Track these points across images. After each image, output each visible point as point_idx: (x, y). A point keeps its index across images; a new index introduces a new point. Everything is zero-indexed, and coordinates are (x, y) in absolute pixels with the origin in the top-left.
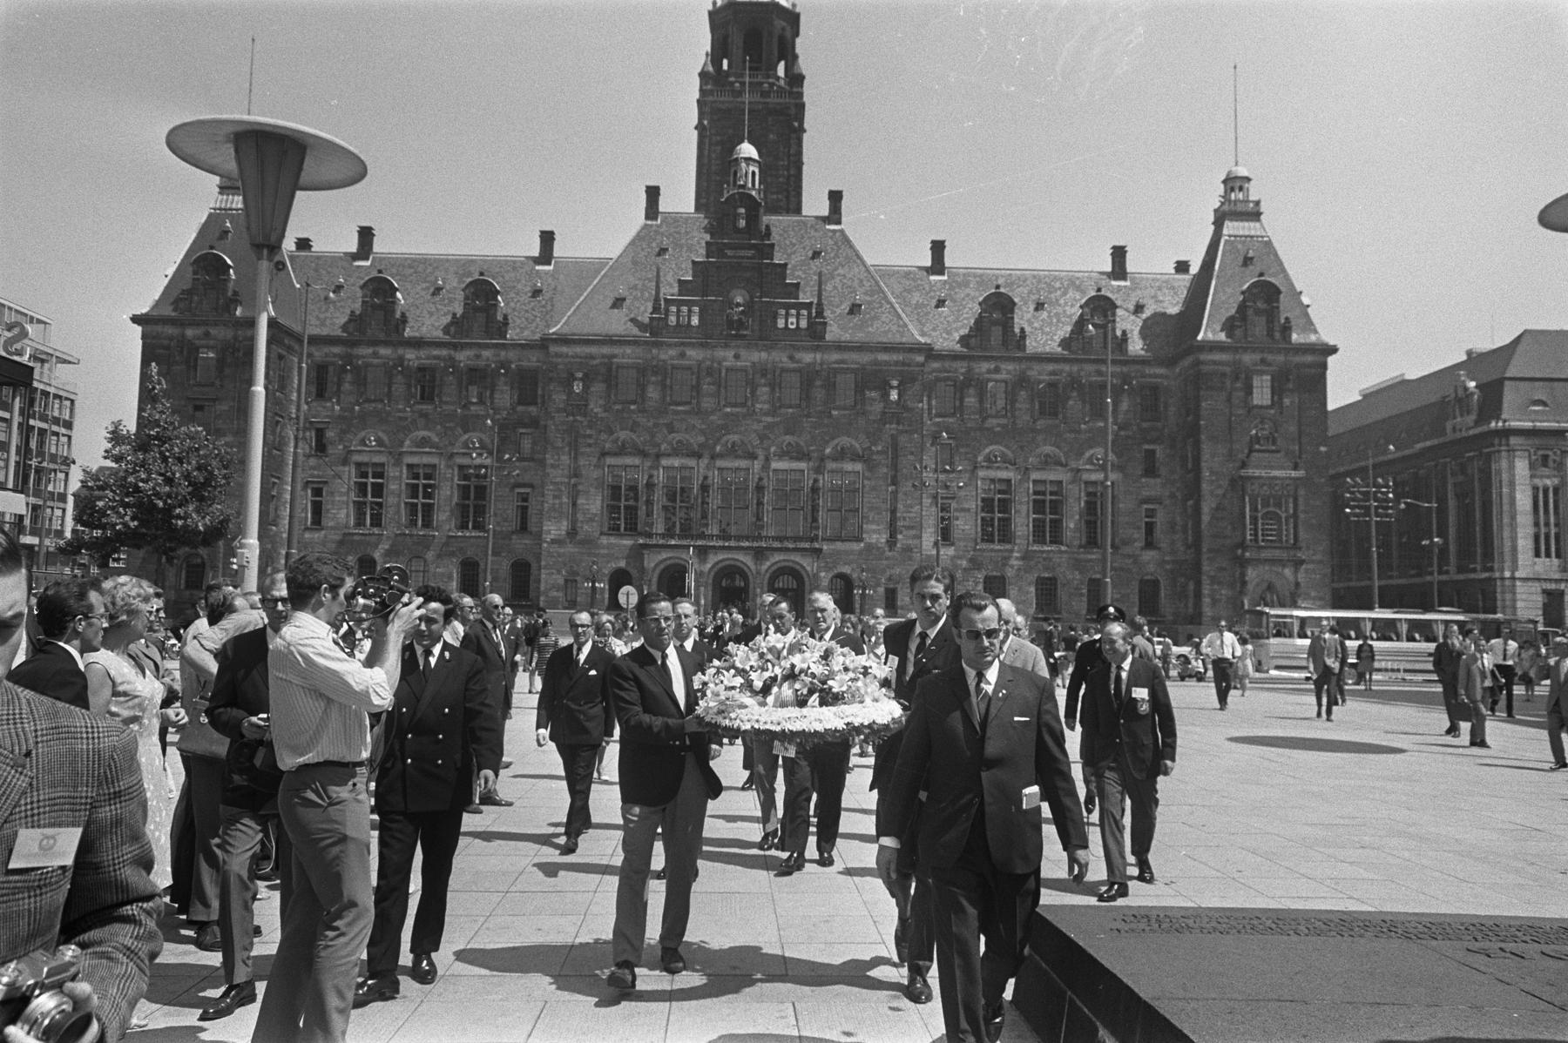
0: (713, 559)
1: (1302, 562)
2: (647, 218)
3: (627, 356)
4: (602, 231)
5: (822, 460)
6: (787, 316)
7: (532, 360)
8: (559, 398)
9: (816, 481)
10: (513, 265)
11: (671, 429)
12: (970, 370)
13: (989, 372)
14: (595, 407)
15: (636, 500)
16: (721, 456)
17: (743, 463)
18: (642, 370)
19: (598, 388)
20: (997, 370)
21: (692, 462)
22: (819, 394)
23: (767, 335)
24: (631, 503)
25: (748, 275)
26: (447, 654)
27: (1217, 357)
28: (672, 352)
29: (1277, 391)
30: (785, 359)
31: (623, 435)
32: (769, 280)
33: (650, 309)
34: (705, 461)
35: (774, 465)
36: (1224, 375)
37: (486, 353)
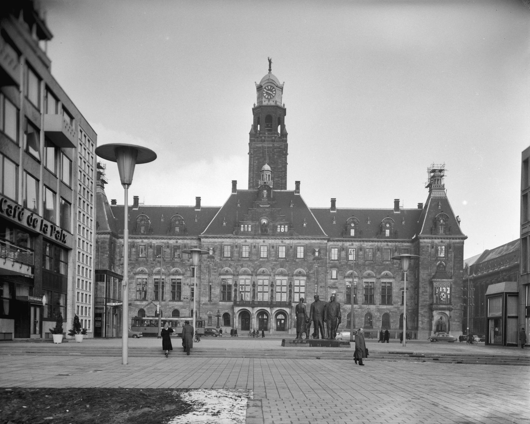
1: (452, 309)
2: (233, 192)
6: (281, 227)
11: (242, 266)
12: (343, 245)
13: (350, 245)
16: (260, 275)
20: (352, 245)
27: (426, 240)
29: (447, 252)
30: (280, 242)
31: (226, 268)
36: (428, 246)
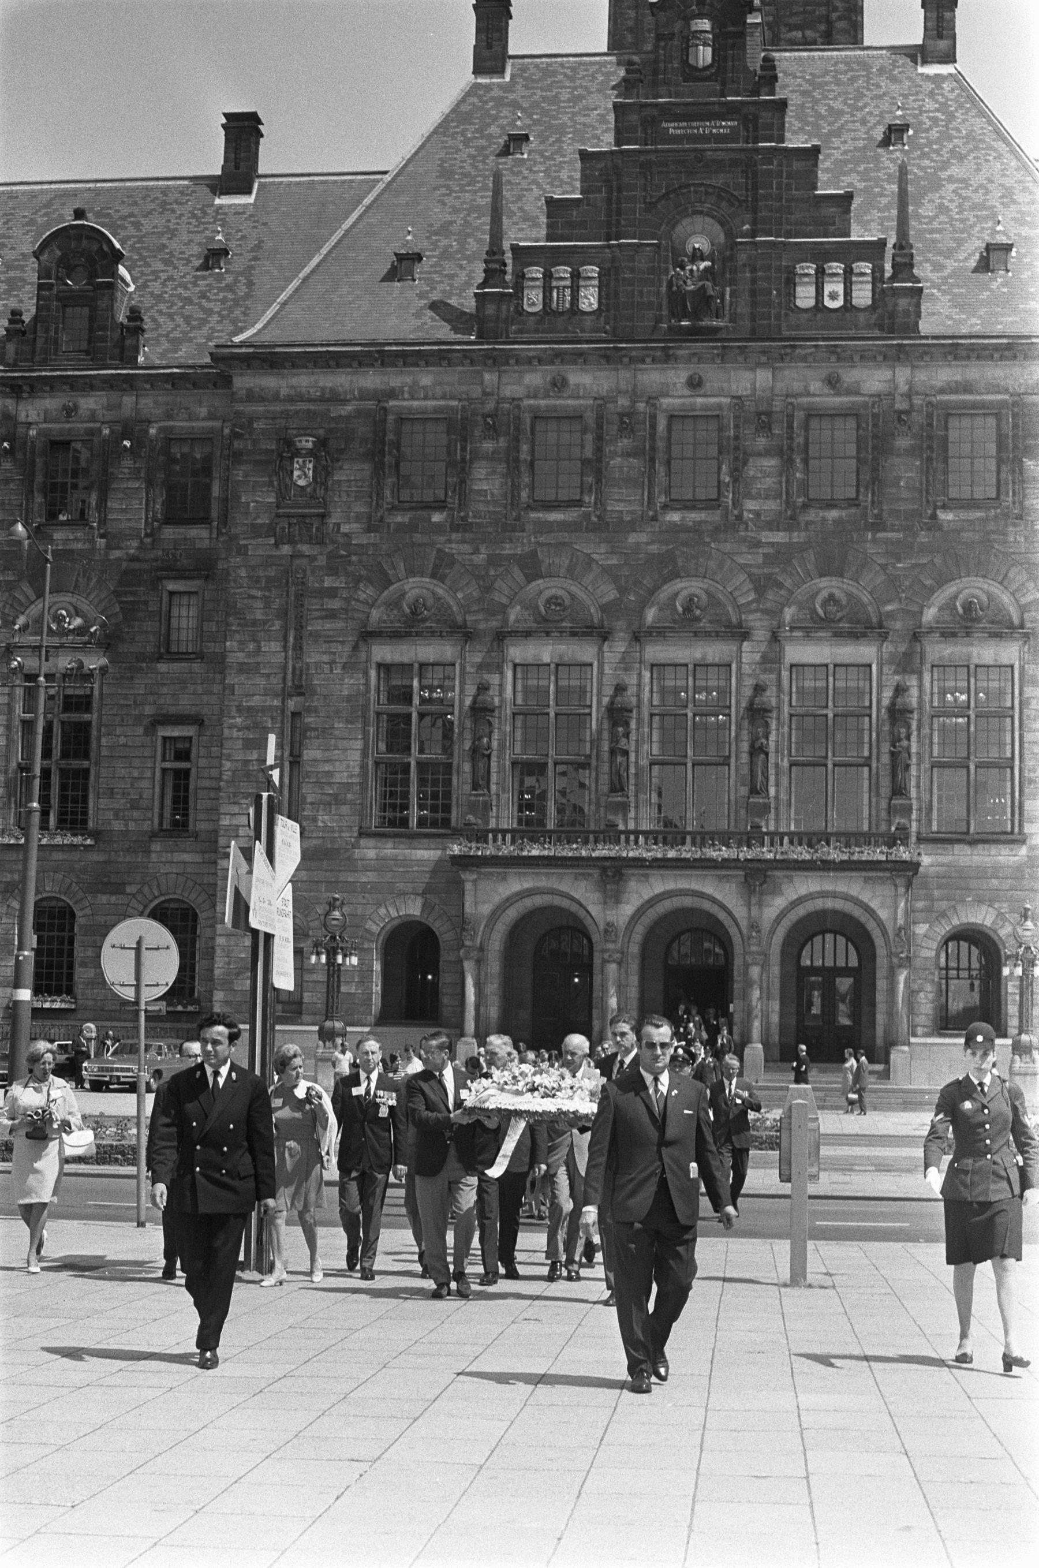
0: (639, 892)
2: (479, 69)
3: (424, 390)
4: (372, 104)
5: (916, 637)
7: (199, 414)
8: (257, 500)
9: (900, 690)
10: (157, 197)
11: (532, 568)
14: (346, 520)
15: (447, 750)
16: (658, 633)
17: (714, 651)
18: (459, 427)
19: (351, 473)
21: (585, 651)
22: (904, 472)
23: (773, 331)
24: (434, 754)
25: (718, 180)
26: (234, 1075)
28: (535, 378)
30: (815, 386)
31: (415, 587)
32: (776, 194)
33: (480, 277)
34: (618, 647)
35: (796, 652)
37: (89, 403)
